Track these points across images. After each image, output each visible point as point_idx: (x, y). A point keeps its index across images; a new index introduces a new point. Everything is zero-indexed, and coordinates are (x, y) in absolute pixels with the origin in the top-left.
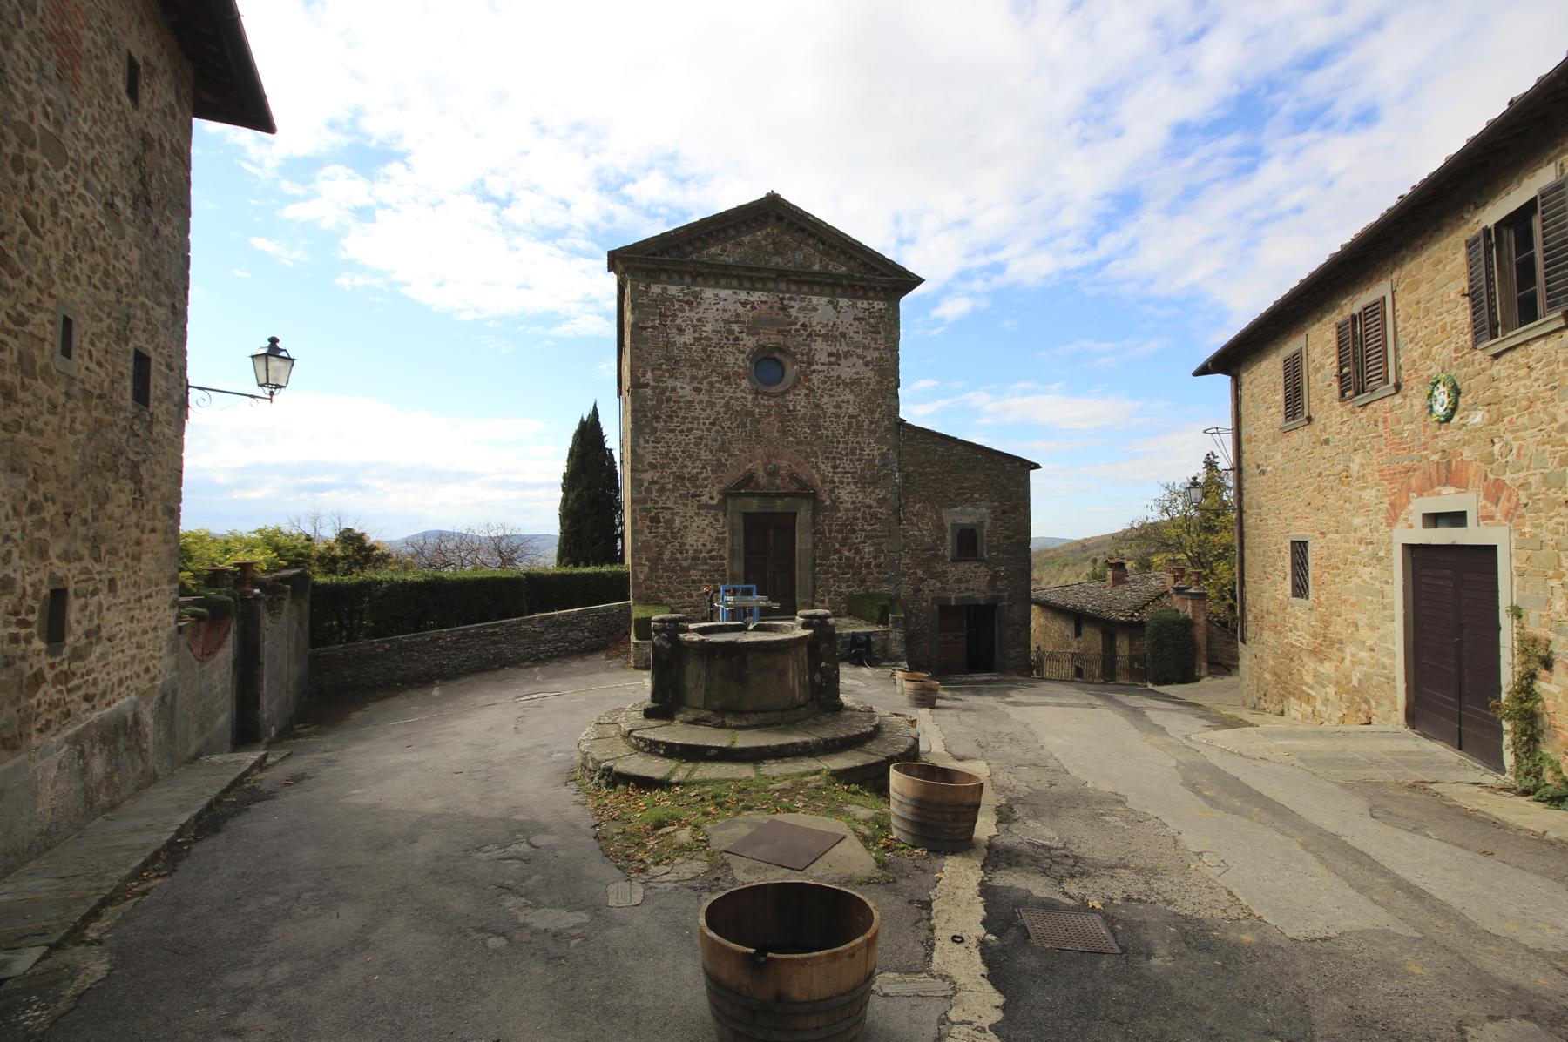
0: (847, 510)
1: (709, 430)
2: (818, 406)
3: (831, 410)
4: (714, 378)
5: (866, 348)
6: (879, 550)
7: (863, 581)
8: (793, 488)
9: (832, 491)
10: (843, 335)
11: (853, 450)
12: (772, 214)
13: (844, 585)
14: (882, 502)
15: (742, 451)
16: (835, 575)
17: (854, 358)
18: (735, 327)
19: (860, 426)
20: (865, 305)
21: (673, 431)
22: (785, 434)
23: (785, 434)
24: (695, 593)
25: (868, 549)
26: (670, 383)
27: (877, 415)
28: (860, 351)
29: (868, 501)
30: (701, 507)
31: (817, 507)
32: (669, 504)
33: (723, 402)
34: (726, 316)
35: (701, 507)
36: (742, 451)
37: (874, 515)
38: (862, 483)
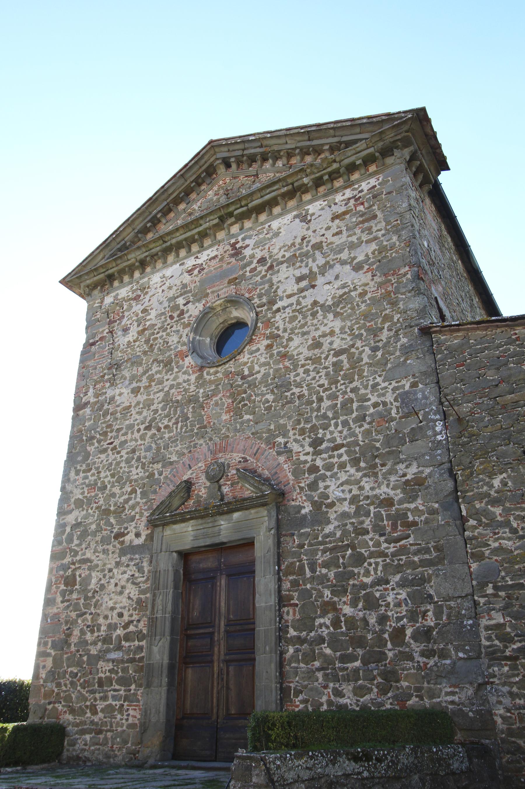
0: (345, 515)
1: (143, 438)
2: (284, 356)
3: (306, 353)
4: (155, 368)
5: (352, 246)
6: (420, 598)
7: (390, 677)
8: (248, 491)
9: (313, 486)
10: (318, 246)
11: (347, 405)
12: (211, 142)
13: (347, 688)
14: (413, 487)
15: (181, 454)
16: (328, 661)
17: (338, 268)
18: (181, 301)
19: (355, 362)
20: (348, 193)
21: (105, 451)
22: (238, 413)
23: (238, 413)
24: (101, 705)
25: (395, 595)
26: (110, 393)
27: (385, 335)
28: (344, 255)
29: (384, 491)
30: (123, 552)
31: (285, 523)
32: (89, 555)
33: (161, 395)
34: (171, 294)
35: (123, 552)
36: (181, 454)
37: (402, 516)
38: (368, 459)
